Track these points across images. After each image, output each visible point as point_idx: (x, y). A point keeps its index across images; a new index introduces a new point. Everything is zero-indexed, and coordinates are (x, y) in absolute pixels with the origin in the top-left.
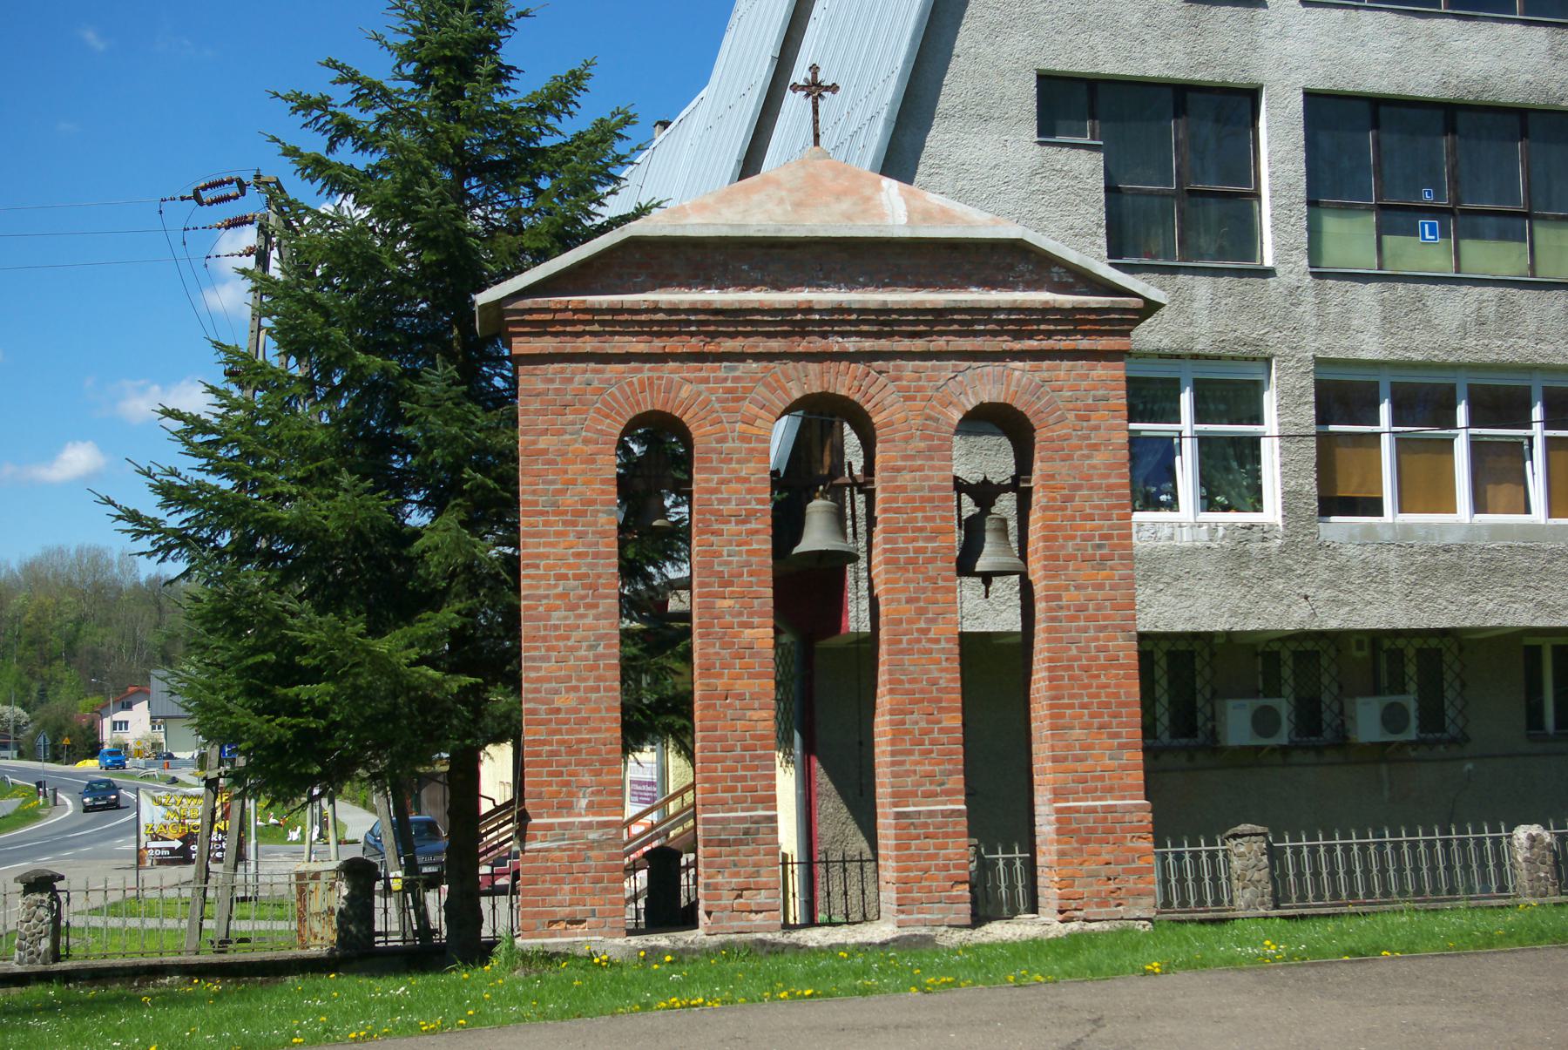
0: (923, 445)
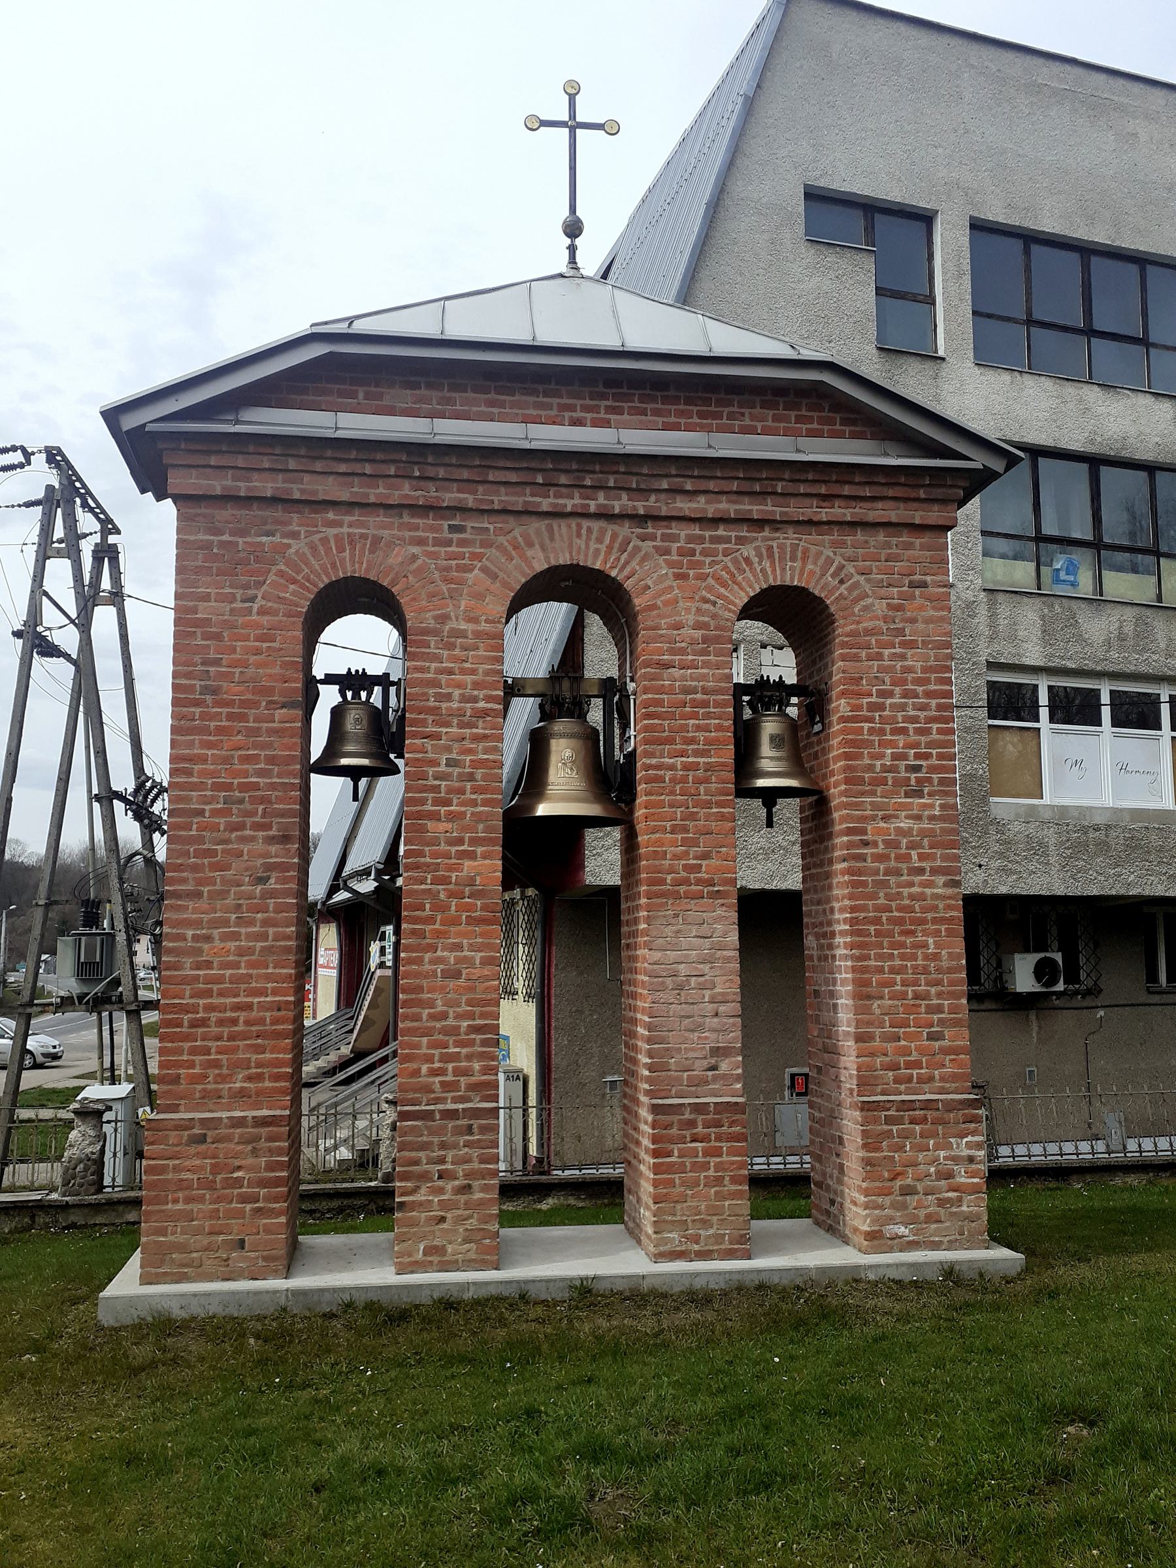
0: (698, 634)
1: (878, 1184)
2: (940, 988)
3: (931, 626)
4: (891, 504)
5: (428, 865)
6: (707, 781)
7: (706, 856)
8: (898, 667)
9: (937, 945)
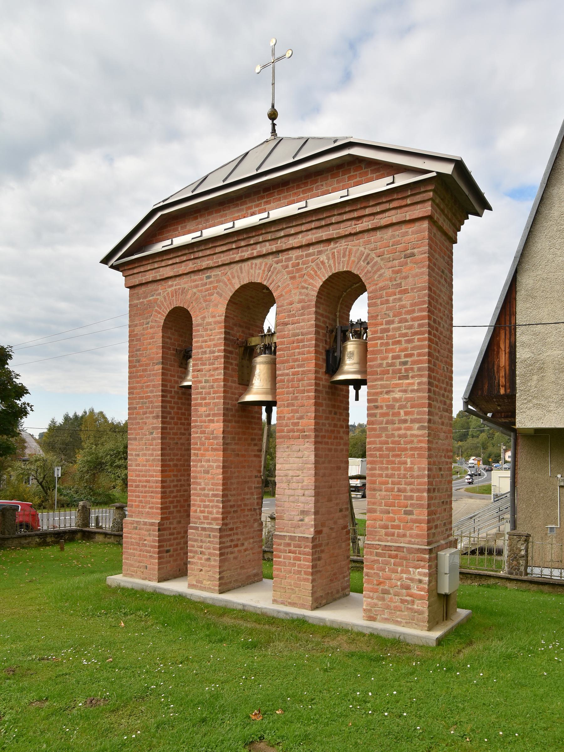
0: (299, 306)
1: (371, 586)
2: (412, 486)
3: (416, 278)
4: (393, 212)
5: (198, 426)
6: (303, 380)
7: (301, 418)
8: (397, 306)
9: (412, 463)
